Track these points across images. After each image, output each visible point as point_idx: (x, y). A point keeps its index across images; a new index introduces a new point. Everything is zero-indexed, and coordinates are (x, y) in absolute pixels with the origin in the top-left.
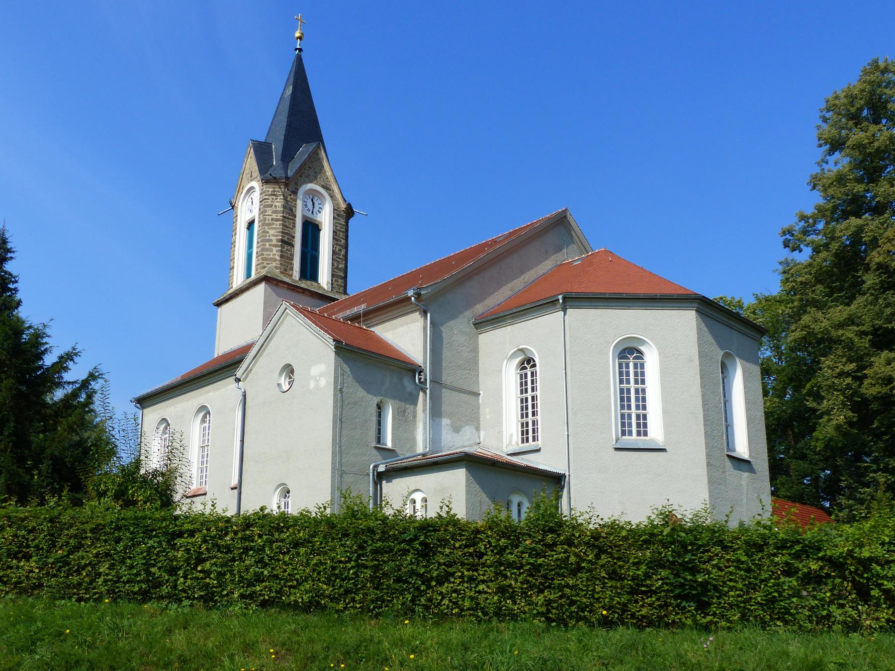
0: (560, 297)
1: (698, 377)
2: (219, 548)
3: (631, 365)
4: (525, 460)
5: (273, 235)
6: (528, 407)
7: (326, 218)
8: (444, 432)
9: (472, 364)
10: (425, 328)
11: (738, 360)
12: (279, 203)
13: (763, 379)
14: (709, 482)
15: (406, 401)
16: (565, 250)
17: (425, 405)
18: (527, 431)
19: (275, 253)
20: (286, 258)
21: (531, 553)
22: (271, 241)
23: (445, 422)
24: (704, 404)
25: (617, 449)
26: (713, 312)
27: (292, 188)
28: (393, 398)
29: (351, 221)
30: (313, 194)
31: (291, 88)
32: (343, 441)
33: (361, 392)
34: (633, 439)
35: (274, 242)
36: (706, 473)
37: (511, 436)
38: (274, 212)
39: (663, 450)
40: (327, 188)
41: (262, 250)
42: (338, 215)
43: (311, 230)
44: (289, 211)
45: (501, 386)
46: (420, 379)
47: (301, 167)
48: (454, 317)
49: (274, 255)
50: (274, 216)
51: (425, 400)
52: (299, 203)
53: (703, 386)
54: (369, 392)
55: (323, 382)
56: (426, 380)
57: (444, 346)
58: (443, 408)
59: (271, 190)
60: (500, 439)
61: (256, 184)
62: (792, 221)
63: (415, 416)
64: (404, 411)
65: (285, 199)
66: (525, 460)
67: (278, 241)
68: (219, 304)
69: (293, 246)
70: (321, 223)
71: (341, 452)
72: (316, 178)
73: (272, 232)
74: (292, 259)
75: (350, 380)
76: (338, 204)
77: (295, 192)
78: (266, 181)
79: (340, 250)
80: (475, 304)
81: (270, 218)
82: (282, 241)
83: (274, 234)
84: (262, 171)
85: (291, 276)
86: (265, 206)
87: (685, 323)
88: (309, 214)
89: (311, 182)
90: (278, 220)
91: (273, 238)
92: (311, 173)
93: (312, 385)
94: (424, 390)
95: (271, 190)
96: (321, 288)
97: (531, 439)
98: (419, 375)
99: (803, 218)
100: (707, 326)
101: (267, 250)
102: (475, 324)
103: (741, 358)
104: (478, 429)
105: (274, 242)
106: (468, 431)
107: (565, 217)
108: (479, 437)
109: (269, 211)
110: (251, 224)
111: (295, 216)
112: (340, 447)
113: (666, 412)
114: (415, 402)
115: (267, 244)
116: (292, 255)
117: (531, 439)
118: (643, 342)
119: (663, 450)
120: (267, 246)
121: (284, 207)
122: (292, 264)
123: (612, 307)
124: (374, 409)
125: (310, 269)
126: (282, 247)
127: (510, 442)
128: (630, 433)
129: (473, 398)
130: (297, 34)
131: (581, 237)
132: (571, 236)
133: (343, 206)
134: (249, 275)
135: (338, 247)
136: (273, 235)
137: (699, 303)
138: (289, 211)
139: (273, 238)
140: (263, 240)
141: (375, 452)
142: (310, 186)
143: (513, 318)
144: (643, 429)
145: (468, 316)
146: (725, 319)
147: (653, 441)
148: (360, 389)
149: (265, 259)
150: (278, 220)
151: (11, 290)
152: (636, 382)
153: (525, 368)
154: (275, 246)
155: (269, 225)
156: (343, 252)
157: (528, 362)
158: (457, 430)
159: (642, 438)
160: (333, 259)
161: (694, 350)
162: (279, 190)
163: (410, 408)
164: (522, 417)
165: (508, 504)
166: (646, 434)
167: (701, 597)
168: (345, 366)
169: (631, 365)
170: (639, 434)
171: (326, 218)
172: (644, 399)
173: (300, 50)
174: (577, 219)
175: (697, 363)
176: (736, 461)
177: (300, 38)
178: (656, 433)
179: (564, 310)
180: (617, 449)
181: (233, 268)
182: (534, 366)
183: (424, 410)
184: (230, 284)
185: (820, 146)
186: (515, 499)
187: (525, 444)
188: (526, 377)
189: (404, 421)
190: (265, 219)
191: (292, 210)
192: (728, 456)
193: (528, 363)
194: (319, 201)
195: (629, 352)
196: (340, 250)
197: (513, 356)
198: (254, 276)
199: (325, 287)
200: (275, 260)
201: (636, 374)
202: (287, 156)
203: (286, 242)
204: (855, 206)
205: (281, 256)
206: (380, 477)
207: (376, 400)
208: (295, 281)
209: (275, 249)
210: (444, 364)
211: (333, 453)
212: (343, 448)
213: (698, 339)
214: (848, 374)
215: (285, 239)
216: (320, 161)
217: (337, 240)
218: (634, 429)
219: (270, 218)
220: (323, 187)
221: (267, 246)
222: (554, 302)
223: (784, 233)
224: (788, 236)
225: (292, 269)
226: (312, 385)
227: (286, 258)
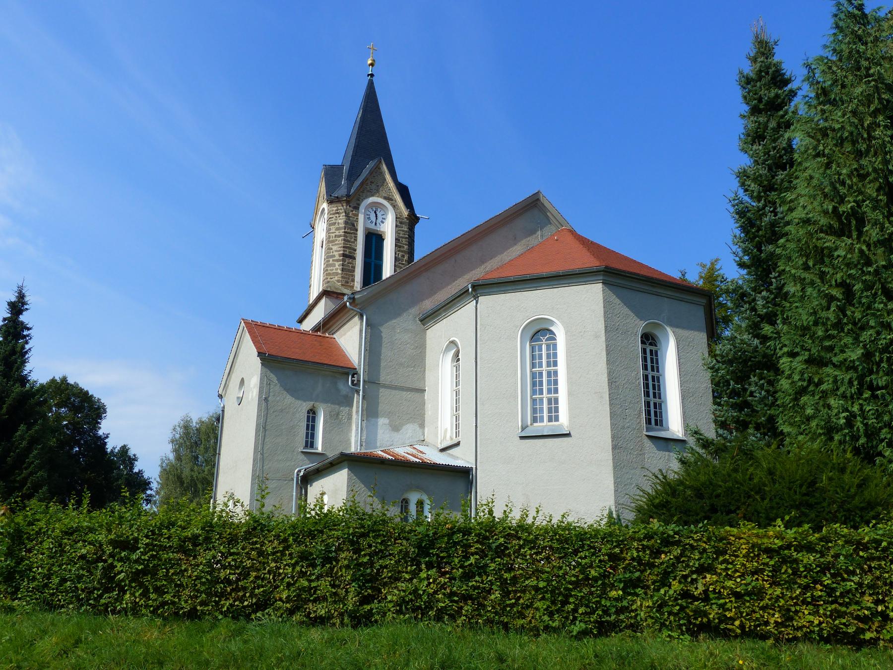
1: (604, 353)
2: (594, 548)
3: (544, 347)
7: (388, 228)
8: (380, 432)
9: (418, 359)
10: (361, 331)
11: (669, 329)
12: (341, 220)
13: (709, 346)
14: (615, 467)
15: (340, 404)
16: (539, 233)
17: (358, 407)
19: (337, 267)
20: (348, 271)
21: (427, 551)
22: (334, 256)
23: (382, 421)
24: (612, 382)
25: (522, 438)
26: (624, 279)
27: (353, 204)
28: (325, 401)
29: (417, 228)
30: (376, 207)
32: (266, 448)
33: (289, 399)
34: (544, 426)
35: (337, 257)
36: (611, 457)
37: (446, 431)
38: (337, 229)
39: (568, 435)
40: (389, 199)
42: (401, 223)
43: (374, 241)
44: (351, 226)
45: (442, 380)
46: (353, 381)
47: (362, 184)
48: (397, 315)
49: (337, 269)
50: (337, 233)
51: (358, 402)
52: (361, 217)
53: (609, 362)
54: (298, 398)
56: (359, 381)
57: (384, 345)
58: (380, 408)
61: (325, 205)
63: (350, 418)
64: (338, 414)
65: (347, 215)
70: (384, 232)
71: (263, 460)
72: (378, 191)
73: (335, 248)
75: (276, 387)
76: (401, 212)
77: (357, 208)
78: (331, 202)
79: (403, 256)
80: (422, 300)
82: (344, 255)
84: (329, 192)
87: (590, 298)
88: (372, 226)
89: (373, 196)
90: (340, 236)
91: (336, 254)
92: (373, 186)
94: (358, 392)
98: (353, 377)
100: (618, 296)
102: (421, 321)
103: (672, 325)
104: (422, 426)
105: (337, 257)
106: (410, 430)
107: (538, 200)
108: (423, 434)
109: (333, 228)
111: (357, 230)
112: (262, 454)
114: (350, 405)
116: (354, 267)
118: (552, 323)
119: (568, 435)
120: (331, 262)
121: (346, 223)
122: (353, 276)
123: (505, 292)
124: (303, 415)
126: (343, 260)
127: (445, 437)
128: (542, 420)
129: (417, 395)
130: (370, 62)
131: (559, 217)
132: (547, 217)
135: (401, 254)
137: (604, 275)
138: (351, 226)
139: (336, 254)
141: (303, 457)
142: (372, 199)
143: (445, 311)
144: (554, 416)
145: (415, 311)
146: (651, 289)
147: (561, 426)
148: (288, 396)
150: (340, 236)
151: (25, 337)
152: (548, 365)
154: (337, 261)
155: (333, 241)
158: (396, 428)
159: (554, 423)
160: (395, 266)
161: (600, 326)
162: (342, 208)
163: (344, 410)
165: (405, 503)
168: (272, 375)
169: (544, 347)
170: (550, 420)
171: (388, 228)
173: (372, 75)
174: (552, 199)
175: (604, 339)
176: (662, 443)
177: (372, 65)
179: (476, 298)
180: (522, 438)
183: (357, 412)
186: (414, 498)
189: (337, 423)
191: (353, 225)
192: (648, 436)
194: (382, 212)
195: (539, 333)
196: (403, 256)
197: (448, 349)
200: (337, 274)
201: (548, 356)
202: (352, 176)
203: (348, 256)
206: (306, 480)
207: (306, 406)
209: (337, 264)
210: (383, 364)
211: (254, 461)
212: (265, 455)
213: (605, 313)
215: (347, 253)
216: (382, 174)
217: (400, 247)
218: (546, 415)
220: (385, 198)
221: (331, 262)
225: (353, 281)
227: (348, 271)
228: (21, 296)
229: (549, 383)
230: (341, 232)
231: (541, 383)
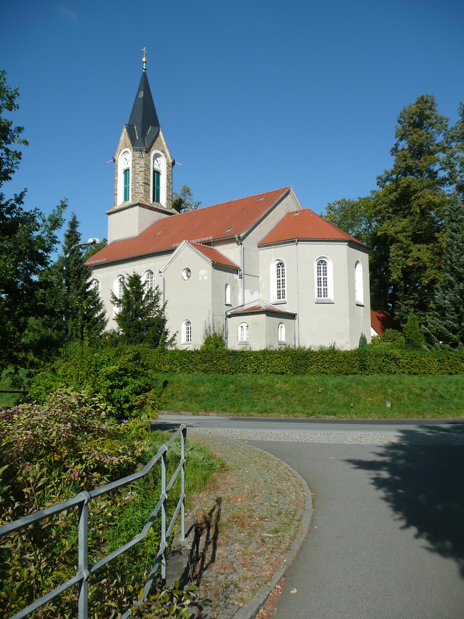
0: (296, 240)
4: (281, 307)
5: (140, 180)
6: (280, 284)
12: (142, 162)
18: (280, 294)
19: (141, 189)
20: (147, 192)
31: (142, 92)
35: (141, 184)
38: (140, 167)
40: (163, 152)
41: (135, 188)
42: (169, 166)
43: (157, 173)
44: (147, 166)
49: (141, 190)
50: (140, 170)
55: (206, 278)
59: (138, 155)
60: (269, 297)
62: (382, 173)
66: (281, 307)
67: (143, 183)
68: (109, 214)
69: (149, 185)
70: (160, 171)
73: (139, 178)
74: (149, 192)
78: (135, 150)
81: (138, 170)
83: (140, 179)
85: (149, 201)
86: (135, 164)
90: (142, 171)
91: (141, 182)
93: (200, 278)
95: (138, 155)
96: (162, 206)
97: (281, 297)
99: (386, 172)
101: (137, 188)
105: (141, 184)
110: (126, 171)
113: (335, 288)
115: (137, 184)
116: (149, 190)
117: (281, 297)
122: (149, 195)
125: (156, 198)
127: (273, 299)
128: (321, 297)
130: (144, 60)
133: (171, 161)
134: (126, 198)
135: (169, 184)
136: (140, 180)
139: (141, 182)
140: (134, 183)
144: (326, 295)
147: (330, 300)
149: (137, 193)
150: (142, 171)
153: (279, 267)
154: (141, 186)
155: (138, 174)
156: (171, 186)
157: (281, 264)
158: (252, 294)
164: (278, 288)
166: (327, 296)
167: (364, 367)
170: (324, 296)
172: (326, 282)
178: (331, 296)
181: (117, 194)
182: (283, 266)
184: (115, 204)
185: (396, 137)
187: (279, 300)
188: (280, 271)
190: (136, 171)
193: (281, 265)
195: (322, 262)
196: (170, 185)
198: (130, 202)
199: (164, 206)
200: (142, 193)
202: (143, 134)
204: (408, 170)
205: (145, 191)
208: (151, 204)
214: (400, 255)
218: (323, 294)
219: (138, 170)
222: (293, 242)
223: (378, 178)
224: (380, 180)
225: (149, 198)
226: (200, 278)
227: (147, 192)
228: (74, 218)
229: (324, 282)
230: (143, 169)
231: (322, 281)
